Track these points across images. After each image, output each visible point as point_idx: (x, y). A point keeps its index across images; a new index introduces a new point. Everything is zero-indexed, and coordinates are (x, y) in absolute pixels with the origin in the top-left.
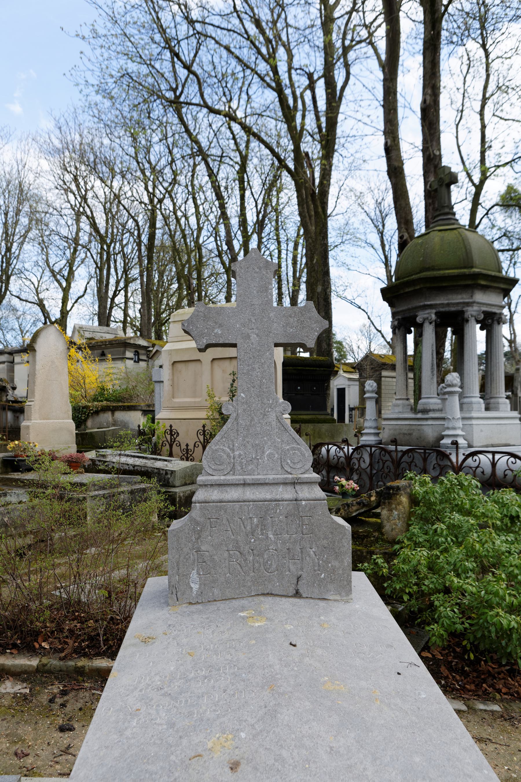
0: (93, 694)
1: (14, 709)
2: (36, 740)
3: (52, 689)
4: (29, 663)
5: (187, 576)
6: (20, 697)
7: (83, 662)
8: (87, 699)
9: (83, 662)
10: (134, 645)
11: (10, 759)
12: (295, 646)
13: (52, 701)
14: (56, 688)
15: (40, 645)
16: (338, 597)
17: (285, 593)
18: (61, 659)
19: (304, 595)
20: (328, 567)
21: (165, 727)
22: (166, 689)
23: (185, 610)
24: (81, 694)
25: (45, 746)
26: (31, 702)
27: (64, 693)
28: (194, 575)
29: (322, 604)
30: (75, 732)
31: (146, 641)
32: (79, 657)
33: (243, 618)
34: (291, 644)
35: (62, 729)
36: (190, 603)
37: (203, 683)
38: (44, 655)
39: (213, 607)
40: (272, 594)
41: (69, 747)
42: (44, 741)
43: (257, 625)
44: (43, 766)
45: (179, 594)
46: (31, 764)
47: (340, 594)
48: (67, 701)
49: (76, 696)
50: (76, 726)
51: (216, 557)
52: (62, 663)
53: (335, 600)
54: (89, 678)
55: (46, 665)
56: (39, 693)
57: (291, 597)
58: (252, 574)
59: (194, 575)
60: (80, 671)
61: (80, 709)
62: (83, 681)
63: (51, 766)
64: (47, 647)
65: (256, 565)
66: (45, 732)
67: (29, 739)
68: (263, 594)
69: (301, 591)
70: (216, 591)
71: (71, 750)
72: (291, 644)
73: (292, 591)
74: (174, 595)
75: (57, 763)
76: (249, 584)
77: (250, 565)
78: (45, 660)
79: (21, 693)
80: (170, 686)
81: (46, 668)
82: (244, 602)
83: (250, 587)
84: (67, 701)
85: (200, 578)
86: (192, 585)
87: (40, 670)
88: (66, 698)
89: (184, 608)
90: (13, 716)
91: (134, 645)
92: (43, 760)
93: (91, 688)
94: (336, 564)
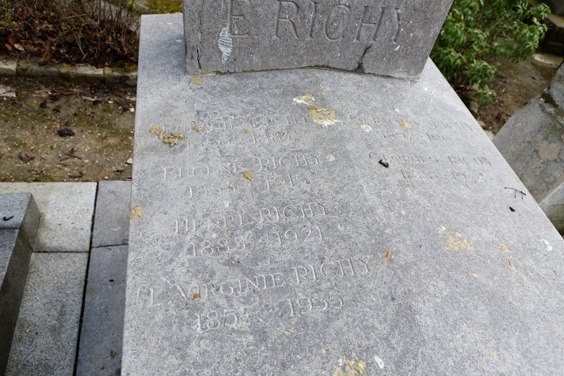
0: (85, 100)
1: (5, 114)
2: (37, 144)
3: (39, 94)
4: (5, 67)
5: (215, 35)
6: (7, 101)
7: (65, 69)
8: (80, 105)
9: (65, 69)
10: (153, 149)
11: (16, 163)
12: (386, 166)
13: (43, 105)
14: (45, 93)
15: (13, 47)
16: (404, 76)
17: (344, 67)
18: (41, 64)
19: (367, 71)
20: (408, 37)
21: (251, 338)
22: (229, 251)
23: (214, 83)
24: (72, 100)
25: (49, 150)
26: (21, 106)
27: (54, 98)
28: (225, 34)
29: (388, 84)
30: (75, 136)
31: (171, 141)
32: (61, 63)
33: (301, 107)
34: (380, 162)
35: (61, 134)
36: (218, 72)
37: (283, 240)
38: (21, 59)
39: (252, 82)
40: (328, 67)
41: (72, 151)
42: (46, 146)
43: (326, 123)
44: (52, 168)
45: (202, 60)
46: (39, 167)
47: (408, 72)
48: (59, 107)
49: (68, 102)
50: (75, 131)
51: (260, 10)
52: (43, 69)
53: (400, 79)
54: (76, 84)
55: (26, 70)
56: (27, 97)
57: (352, 71)
58: (308, 39)
59: (225, 34)
60: (66, 77)
61: (75, 115)
62: (71, 86)
63: (60, 169)
64: (21, 49)
65: (317, 26)
66: (45, 136)
67: (30, 141)
68: (317, 67)
69: (365, 66)
70: (255, 59)
71: (76, 154)
72: (380, 162)
73: (354, 65)
74: (188, 56)
75: (65, 165)
76: (302, 52)
77: (308, 26)
78: (23, 65)
79: (7, 97)
80: (233, 244)
81: (27, 72)
82: (293, 77)
83: (302, 57)
84: (59, 107)
85: (234, 40)
86: (222, 49)
87: (20, 74)
88: (57, 103)
89: (208, 80)
90: (6, 121)
91: (153, 149)
92: (50, 163)
93: (81, 94)
94: (420, 33)
